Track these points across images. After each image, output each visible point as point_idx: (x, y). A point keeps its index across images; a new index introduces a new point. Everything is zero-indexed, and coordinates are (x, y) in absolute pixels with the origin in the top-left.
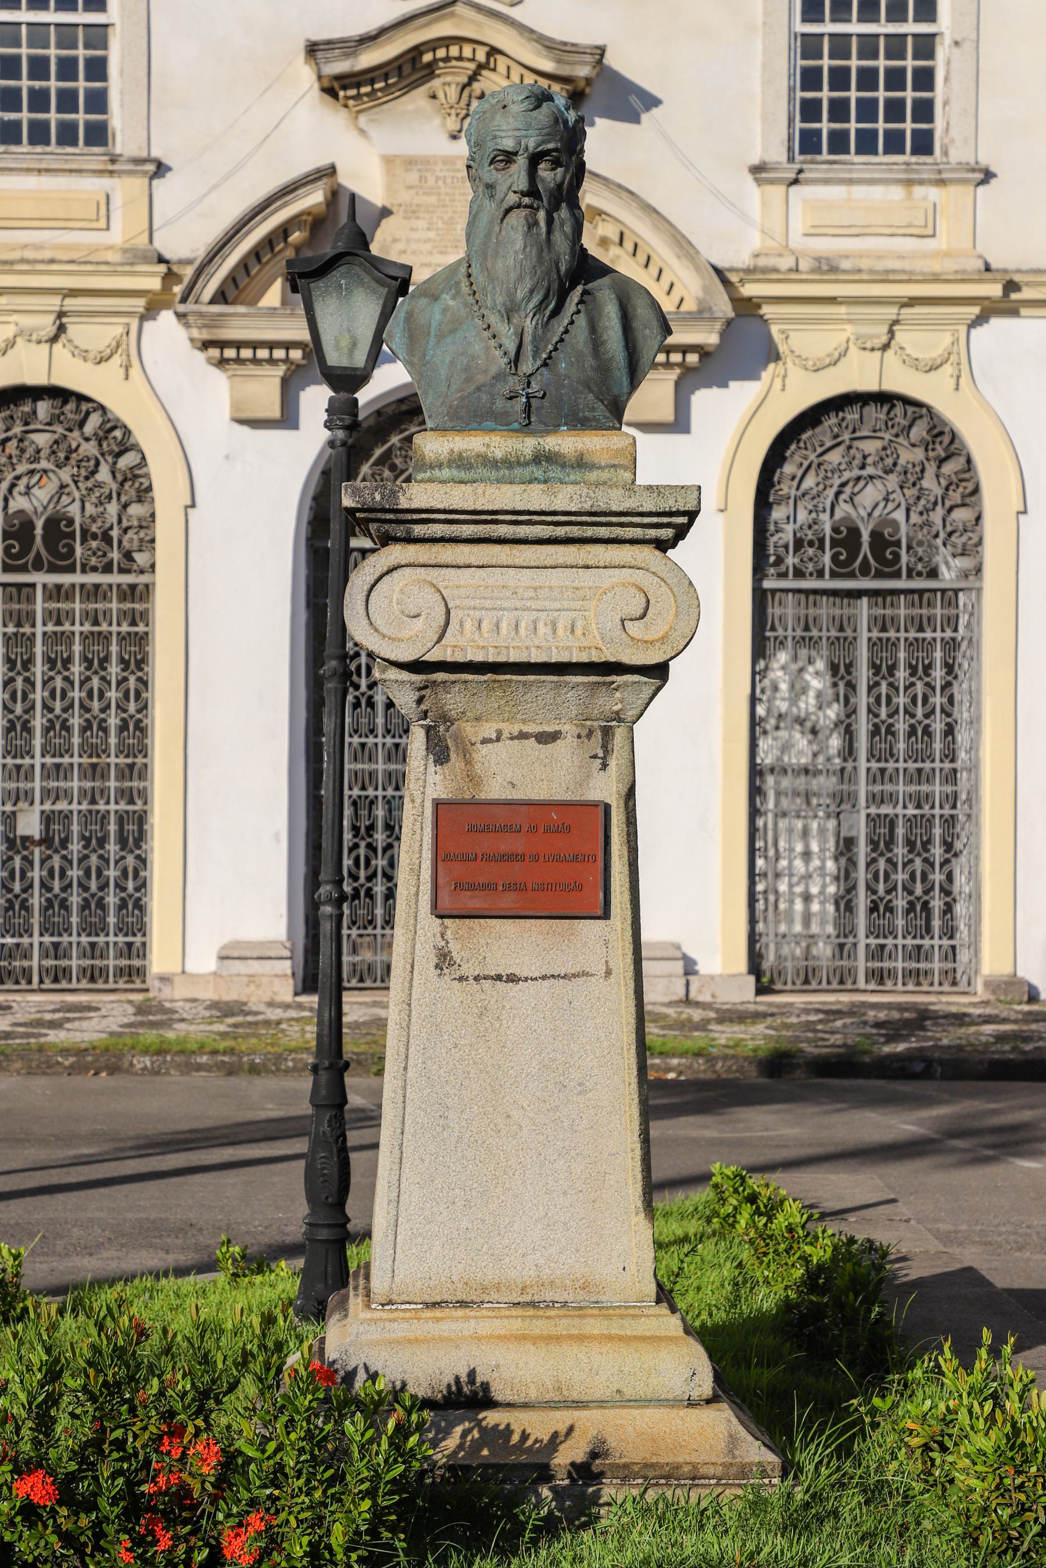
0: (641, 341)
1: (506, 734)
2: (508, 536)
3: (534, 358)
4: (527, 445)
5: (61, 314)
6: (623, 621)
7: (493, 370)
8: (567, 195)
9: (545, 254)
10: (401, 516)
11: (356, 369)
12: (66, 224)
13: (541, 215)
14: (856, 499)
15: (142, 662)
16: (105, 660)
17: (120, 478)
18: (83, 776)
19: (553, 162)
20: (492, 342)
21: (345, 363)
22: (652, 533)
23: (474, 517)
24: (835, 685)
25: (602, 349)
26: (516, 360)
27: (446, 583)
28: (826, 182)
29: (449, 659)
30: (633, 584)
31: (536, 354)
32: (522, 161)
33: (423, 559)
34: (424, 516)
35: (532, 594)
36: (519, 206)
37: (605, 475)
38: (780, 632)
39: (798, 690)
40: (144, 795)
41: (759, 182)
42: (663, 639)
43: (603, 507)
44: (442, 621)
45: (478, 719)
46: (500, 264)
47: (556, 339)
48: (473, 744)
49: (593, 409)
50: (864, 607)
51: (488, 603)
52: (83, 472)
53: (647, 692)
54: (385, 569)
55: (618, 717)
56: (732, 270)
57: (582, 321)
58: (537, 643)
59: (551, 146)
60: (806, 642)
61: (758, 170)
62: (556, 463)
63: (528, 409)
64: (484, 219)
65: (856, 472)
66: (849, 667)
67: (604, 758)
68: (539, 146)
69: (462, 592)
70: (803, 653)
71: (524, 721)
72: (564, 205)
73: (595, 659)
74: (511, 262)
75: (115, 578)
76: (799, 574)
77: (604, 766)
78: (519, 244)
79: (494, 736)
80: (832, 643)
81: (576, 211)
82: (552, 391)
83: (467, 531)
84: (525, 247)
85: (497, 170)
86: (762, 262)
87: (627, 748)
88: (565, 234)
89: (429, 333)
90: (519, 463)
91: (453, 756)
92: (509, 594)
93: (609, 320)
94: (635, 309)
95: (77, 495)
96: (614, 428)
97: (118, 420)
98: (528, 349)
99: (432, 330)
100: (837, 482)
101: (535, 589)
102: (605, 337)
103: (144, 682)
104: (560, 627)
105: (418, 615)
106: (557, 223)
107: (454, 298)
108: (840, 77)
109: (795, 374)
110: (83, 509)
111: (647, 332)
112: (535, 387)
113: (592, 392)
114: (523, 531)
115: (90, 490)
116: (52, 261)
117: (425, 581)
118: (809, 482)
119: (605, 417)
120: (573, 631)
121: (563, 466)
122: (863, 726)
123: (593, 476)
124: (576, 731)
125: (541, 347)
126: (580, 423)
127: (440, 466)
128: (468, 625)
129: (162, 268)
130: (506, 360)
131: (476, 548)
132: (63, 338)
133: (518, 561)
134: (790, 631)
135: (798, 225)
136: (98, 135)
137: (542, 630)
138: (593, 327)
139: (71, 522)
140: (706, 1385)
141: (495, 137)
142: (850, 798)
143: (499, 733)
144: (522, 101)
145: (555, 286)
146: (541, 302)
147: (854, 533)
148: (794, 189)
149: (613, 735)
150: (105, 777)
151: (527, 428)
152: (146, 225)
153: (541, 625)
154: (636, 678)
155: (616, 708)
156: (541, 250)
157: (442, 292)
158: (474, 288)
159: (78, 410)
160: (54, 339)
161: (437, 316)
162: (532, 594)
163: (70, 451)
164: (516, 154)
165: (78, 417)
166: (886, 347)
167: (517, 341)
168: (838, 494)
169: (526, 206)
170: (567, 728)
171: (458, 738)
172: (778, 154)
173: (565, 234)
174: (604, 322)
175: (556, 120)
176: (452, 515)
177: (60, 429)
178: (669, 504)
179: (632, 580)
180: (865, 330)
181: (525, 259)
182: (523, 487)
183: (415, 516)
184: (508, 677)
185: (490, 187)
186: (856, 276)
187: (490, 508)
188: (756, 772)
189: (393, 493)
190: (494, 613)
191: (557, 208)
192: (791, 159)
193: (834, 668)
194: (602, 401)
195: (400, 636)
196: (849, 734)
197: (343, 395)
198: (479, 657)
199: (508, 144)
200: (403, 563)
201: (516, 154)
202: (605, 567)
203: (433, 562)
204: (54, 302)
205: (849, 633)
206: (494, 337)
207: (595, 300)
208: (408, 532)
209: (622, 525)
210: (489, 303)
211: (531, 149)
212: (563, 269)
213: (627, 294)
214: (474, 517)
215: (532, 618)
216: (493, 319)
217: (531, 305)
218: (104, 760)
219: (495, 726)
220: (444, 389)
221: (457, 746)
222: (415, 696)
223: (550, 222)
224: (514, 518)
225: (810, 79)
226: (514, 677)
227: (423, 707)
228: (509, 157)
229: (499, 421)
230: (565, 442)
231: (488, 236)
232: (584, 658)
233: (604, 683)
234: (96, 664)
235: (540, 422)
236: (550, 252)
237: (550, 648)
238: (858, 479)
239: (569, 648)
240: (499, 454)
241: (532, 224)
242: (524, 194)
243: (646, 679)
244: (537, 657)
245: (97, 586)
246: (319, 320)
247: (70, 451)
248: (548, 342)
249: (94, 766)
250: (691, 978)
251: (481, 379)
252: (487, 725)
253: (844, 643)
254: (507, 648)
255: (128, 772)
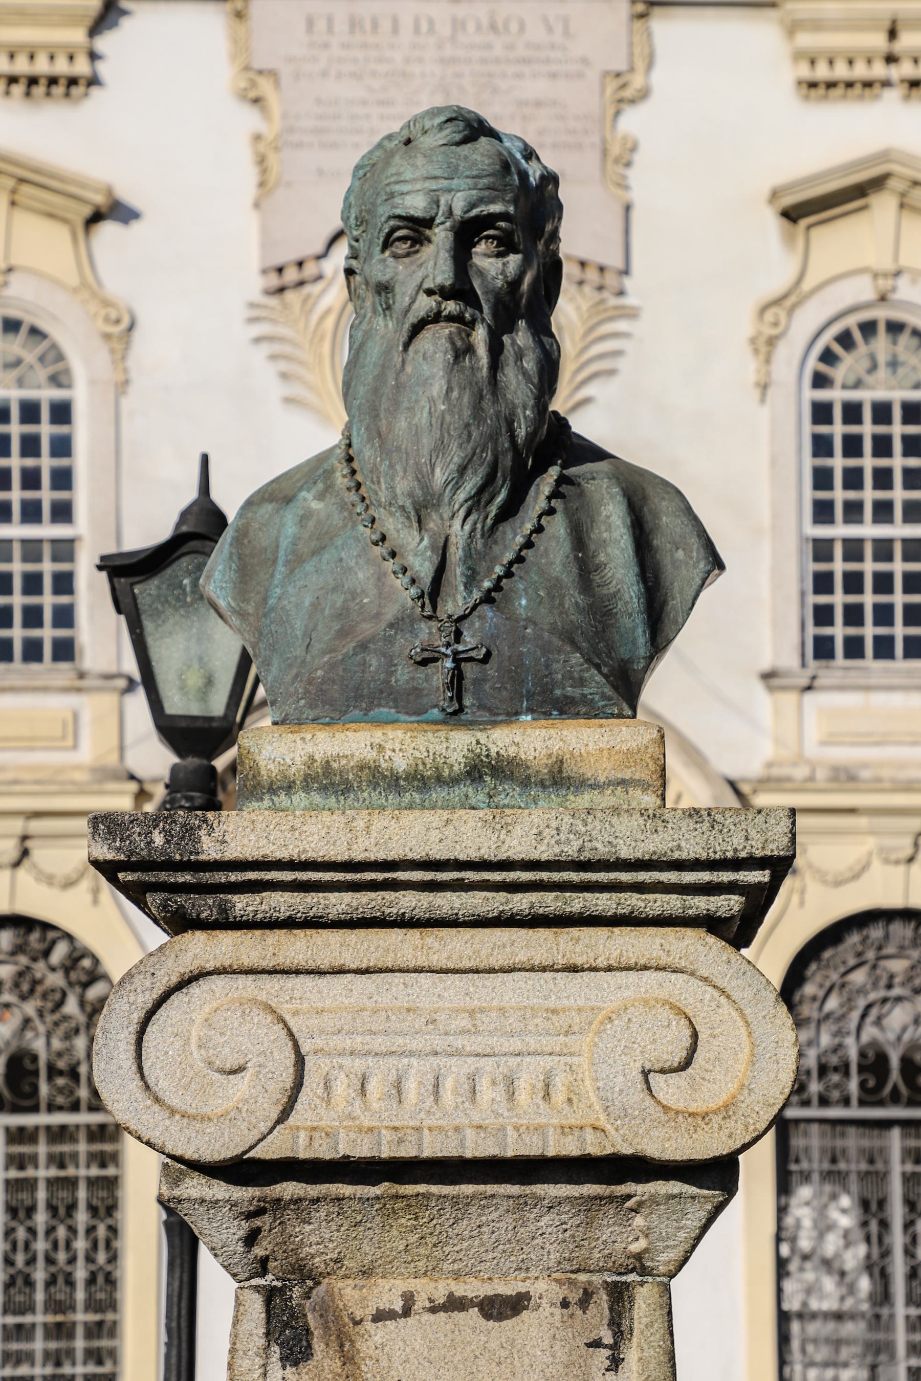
0: (668, 571)
1: (421, 1302)
2: (419, 914)
3: (468, 586)
4: (456, 746)
5: (25, 838)
6: (645, 1074)
7: (391, 612)
8: (531, 303)
9: (487, 404)
10: (208, 877)
11: (211, 719)
12: (30, 743)
13: (480, 335)
14: (885, 1022)
15: (111, 1209)
16: (71, 1207)
17: (89, 1009)
18: (48, 1336)
20: (390, 565)
21: (195, 710)
22: (701, 904)
23: (350, 876)
24: (865, 1224)
25: (597, 578)
27: (296, 1005)
28: (841, 688)
29: (302, 1155)
30: (665, 1002)
31: (471, 580)
32: (441, 236)
33: (249, 959)
34: (252, 875)
35: (463, 1022)
36: (436, 317)
37: (606, 799)
38: (805, 1165)
39: (823, 1228)
40: (113, 1354)
41: (771, 689)
42: (727, 1110)
43: (602, 851)
44: (287, 1078)
45: (366, 1273)
46: (402, 424)
47: (509, 556)
48: (357, 1323)
49: (582, 682)
50: (895, 1139)
51: (379, 1043)
52: (49, 1005)
53: (696, 1215)
54: (175, 979)
55: (639, 1265)
56: (745, 780)
57: (558, 527)
58: (476, 1118)
60: (835, 1177)
61: (768, 676)
62: (511, 777)
63: (457, 682)
64: (374, 351)
65: (882, 993)
66: (882, 1203)
67: (615, 1347)
68: (472, 206)
69: (328, 1021)
70: (828, 1188)
71: (457, 1275)
72: (522, 324)
73: (594, 1150)
74: (422, 417)
75: (84, 1118)
76: (824, 1101)
77: (615, 1363)
78: (438, 387)
79: (398, 1306)
80: (864, 1176)
82: (503, 649)
83: (338, 904)
84: (449, 390)
85: (396, 256)
86: (776, 772)
87: (659, 1326)
88: (525, 373)
89: (275, 561)
91: (318, 1346)
92: (419, 1023)
93: (609, 528)
94: (656, 516)
95: (42, 1029)
97: (86, 948)
98: (456, 572)
99: (281, 553)
100: (861, 1003)
101: (472, 1013)
102: (602, 558)
103: (113, 1230)
104: (523, 1085)
105: (240, 1069)
107: (320, 497)
108: (853, 583)
109: (814, 889)
110: (48, 1044)
111: (680, 554)
112: (469, 640)
113: (578, 649)
114: (447, 903)
115: (56, 1024)
116: (15, 782)
117: (254, 1001)
118: (832, 1004)
119: (604, 697)
120: (547, 1096)
121: (526, 783)
122: (899, 1268)
123: (584, 800)
124: (559, 1292)
125: (482, 567)
126: (557, 705)
128: (342, 1088)
129: (133, 787)
130: (413, 591)
131: (353, 936)
132: (26, 863)
133: (438, 960)
134: (816, 1164)
135: (813, 732)
136: (65, 651)
137: (487, 1093)
138: (579, 539)
139: (35, 1058)
142: (888, 1348)
143: (409, 1300)
144: (441, 127)
145: (507, 461)
146: (481, 490)
147: (882, 1059)
148: (809, 697)
149: (632, 1300)
150: (71, 1336)
151: (455, 716)
152: (115, 742)
153: (484, 1084)
154: (675, 1187)
155: (636, 1247)
156: (479, 397)
157: (301, 489)
158: (359, 477)
159: (43, 939)
160: (17, 864)
161: (290, 529)
162: (463, 1022)
163: (35, 983)
164: (428, 223)
165: (45, 946)
166: (911, 860)
167: (436, 560)
168: (864, 1016)
169: (451, 318)
170: (543, 1288)
171: (326, 1310)
172: (789, 660)
173: (525, 373)
174: (600, 533)
176: (306, 875)
177: (23, 960)
178: (733, 843)
179: (663, 994)
180: (889, 842)
181: (450, 410)
182: (446, 814)
183: (235, 877)
184: (422, 1188)
185: (384, 289)
186: (877, 785)
187: (381, 856)
188: (783, 1318)
189: (189, 831)
190: (392, 1061)
191: (511, 328)
192: (804, 665)
193: (865, 1204)
194: (598, 667)
195: (206, 1110)
196: (882, 1277)
197: (193, 762)
198: (362, 1150)
199: (416, 205)
200: (210, 966)
201: (428, 223)
202: (609, 969)
203: (268, 963)
204: (17, 826)
205: (879, 1166)
206: (393, 554)
207: (582, 494)
208: (224, 909)
209: (639, 888)
210: (383, 496)
211: (458, 212)
212: (522, 432)
213: (642, 495)
214: (350, 876)
215: (466, 1070)
216: (392, 524)
217: (462, 495)
218: (71, 1317)
219: (402, 1285)
220: (299, 651)
221: (326, 1327)
222: (241, 1229)
223: (496, 349)
224: (428, 876)
225: (823, 583)
226: (434, 1189)
227: (258, 1251)
228: (417, 229)
230: (529, 740)
231: (381, 378)
232: (571, 1148)
233: (611, 1199)
234: (62, 1211)
235: (482, 707)
237: (503, 1129)
238: (885, 1000)
239: (540, 1129)
240: (401, 764)
242: (445, 293)
243: (693, 1190)
244: (476, 1147)
245: (63, 1128)
246: (150, 641)
247: (35, 983)
248: (494, 560)
249: (59, 1325)
251: (367, 629)
252: (384, 1284)
253: (875, 1177)
254: (417, 1129)
255: (95, 1330)
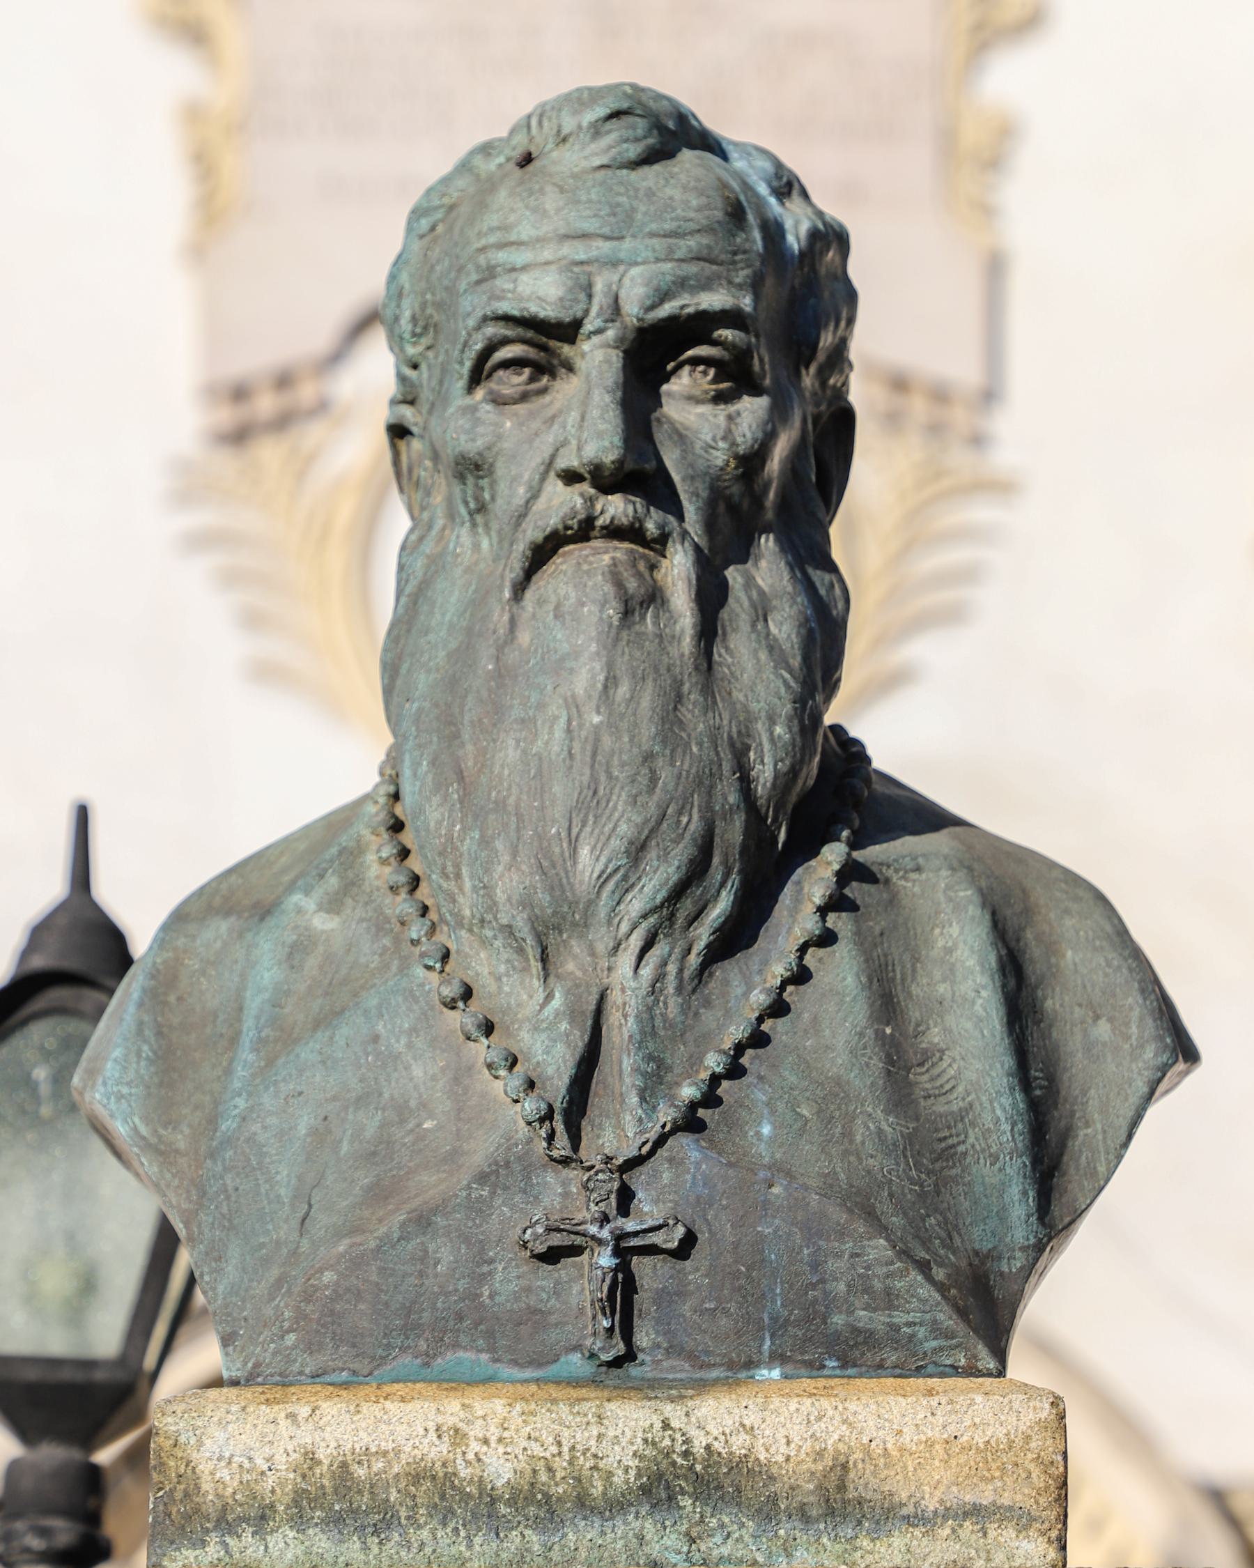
4: (621, 1431)
7: (481, 1150)
9: (691, 712)
11: (90, 1364)
13: (678, 568)
19: (722, 369)
20: (481, 1050)
21: (57, 1343)
25: (922, 1079)
26: (577, 1105)
31: (654, 1082)
36: (584, 530)
46: (509, 753)
47: (737, 1032)
49: (889, 1300)
57: (840, 970)
59: (714, 300)
62: (736, 1499)
63: (622, 1297)
64: (450, 599)
68: (664, 296)
72: (767, 543)
74: (552, 740)
78: (585, 676)
81: (820, 578)
82: (719, 1230)
84: (611, 682)
85: (498, 401)
88: (773, 647)
90: (583, 1503)
93: (950, 975)
94: (1052, 949)
96: (972, 1371)
98: (622, 1066)
99: (248, 1023)
102: (935, 1036)
106: (738, 604)
107: (333, 905)
111: (1103, 1030)
113: (883, 1229)
119: (936, 1330)
121: (768, 1512)
125: (678, 1056)
126: (836, 1348)
127: (262, 1519)
130: (531, 1106)
138: (887, 998)
140: (741, 450)
141: (490, 273)
144: (596, 130)
145: (733, 833)
146: (678, 893)
157: (291, 888)
161: (268, 973)
164: (569, 331)
167: (580, 1040)
169: (615, 532)
173: (773, 647)
174: (929, 985)
175: (736, 214)
185: (472, 469)
191: (743, 552)
194: (924, 1267)
197: (53, 1454)
199: (542, 293)
201: (569, 331)
206: (488, 1028)
207: (893, 902)
211: (632, 309)
212: (765, 773)
216: (485, 964)
217: (636, 904)
220: (285, 1231)
223: (711, 596)
228: (543, 344)
229: (516, 1348)
235: (673, 1350)
236: (710, 704)
240: (501, 1470)
241: (641, 602)
242: (606, 480)
248: (704, 1042)
250: (402, 445)
251: (430, 1185)
